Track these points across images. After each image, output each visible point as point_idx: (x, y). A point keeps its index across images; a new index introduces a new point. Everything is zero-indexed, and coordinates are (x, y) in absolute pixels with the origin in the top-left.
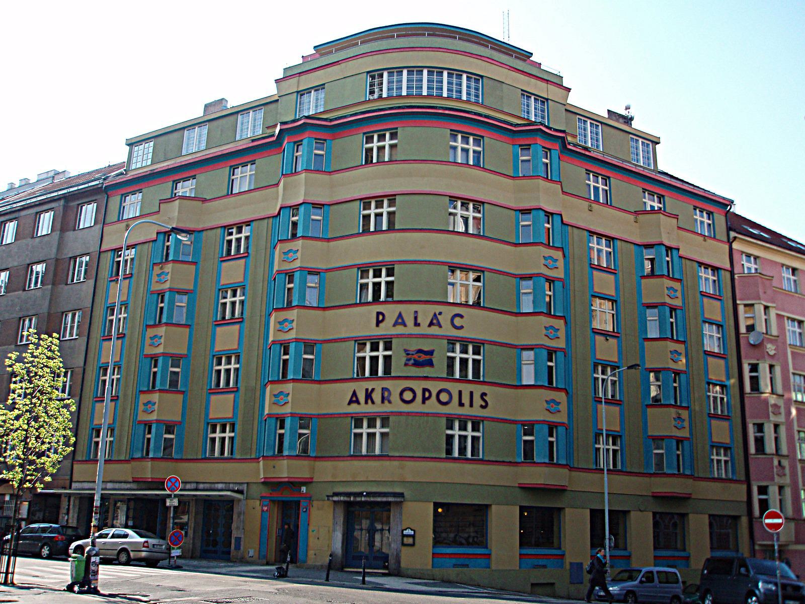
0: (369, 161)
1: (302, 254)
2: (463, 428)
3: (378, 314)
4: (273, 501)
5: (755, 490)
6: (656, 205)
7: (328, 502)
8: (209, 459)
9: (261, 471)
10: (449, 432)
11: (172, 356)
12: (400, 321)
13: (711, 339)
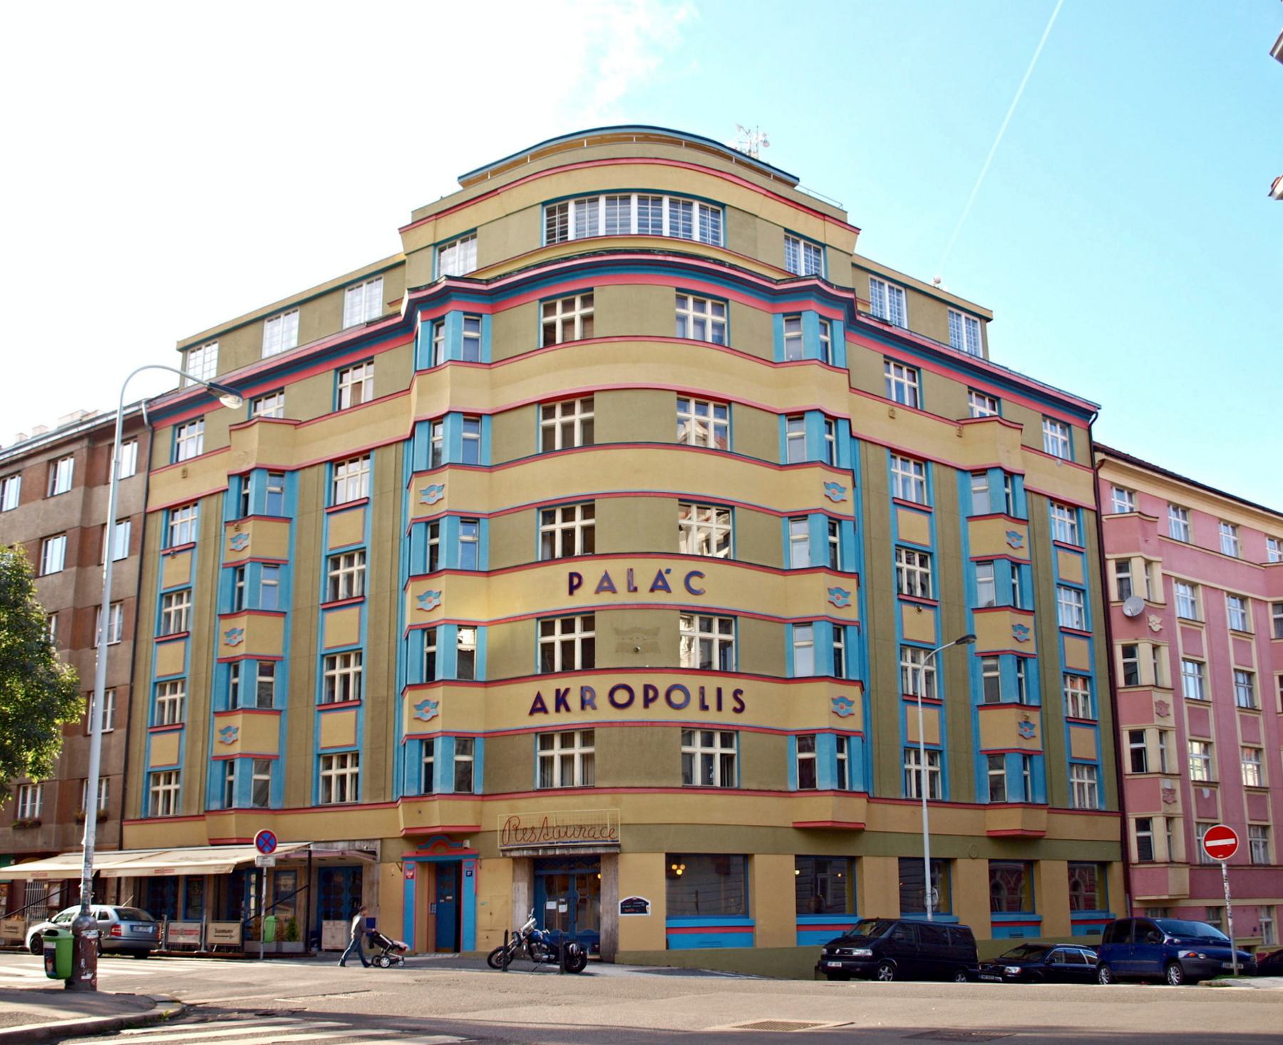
0: (549, 340)
1: (453, 492)
2: (708, 742)
3: (572, 575)
4: (422, 864)
5: (1132, 825)
6: (988, 411)
7: (505, 860)
9: (400, 820)
10: (686, 749)
11: (259, 658)
12: (606, 584)
13: (1069, 612)
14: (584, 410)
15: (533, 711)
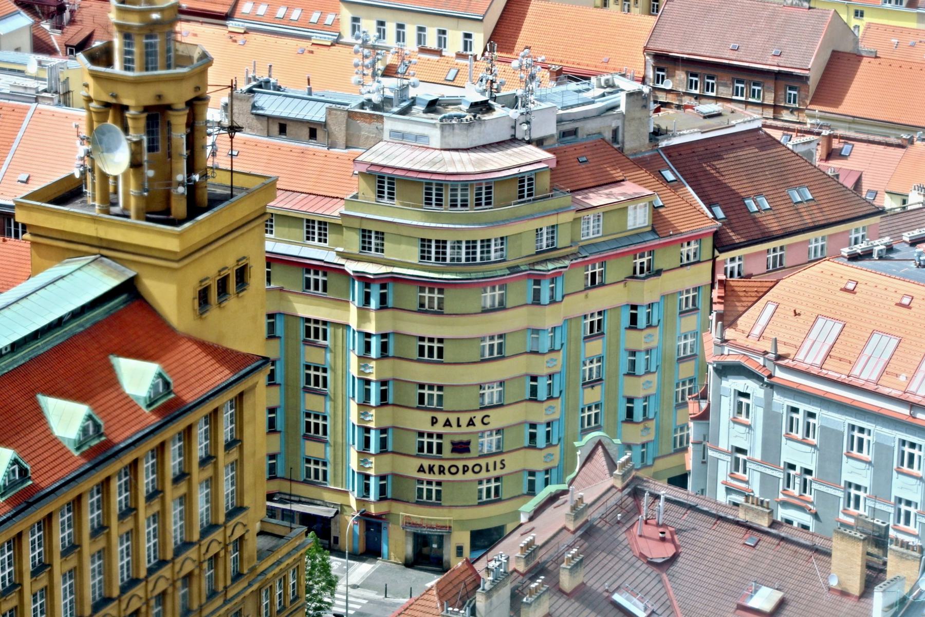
3: (433, 418)
14: (439, 293)
15: (419, 471)
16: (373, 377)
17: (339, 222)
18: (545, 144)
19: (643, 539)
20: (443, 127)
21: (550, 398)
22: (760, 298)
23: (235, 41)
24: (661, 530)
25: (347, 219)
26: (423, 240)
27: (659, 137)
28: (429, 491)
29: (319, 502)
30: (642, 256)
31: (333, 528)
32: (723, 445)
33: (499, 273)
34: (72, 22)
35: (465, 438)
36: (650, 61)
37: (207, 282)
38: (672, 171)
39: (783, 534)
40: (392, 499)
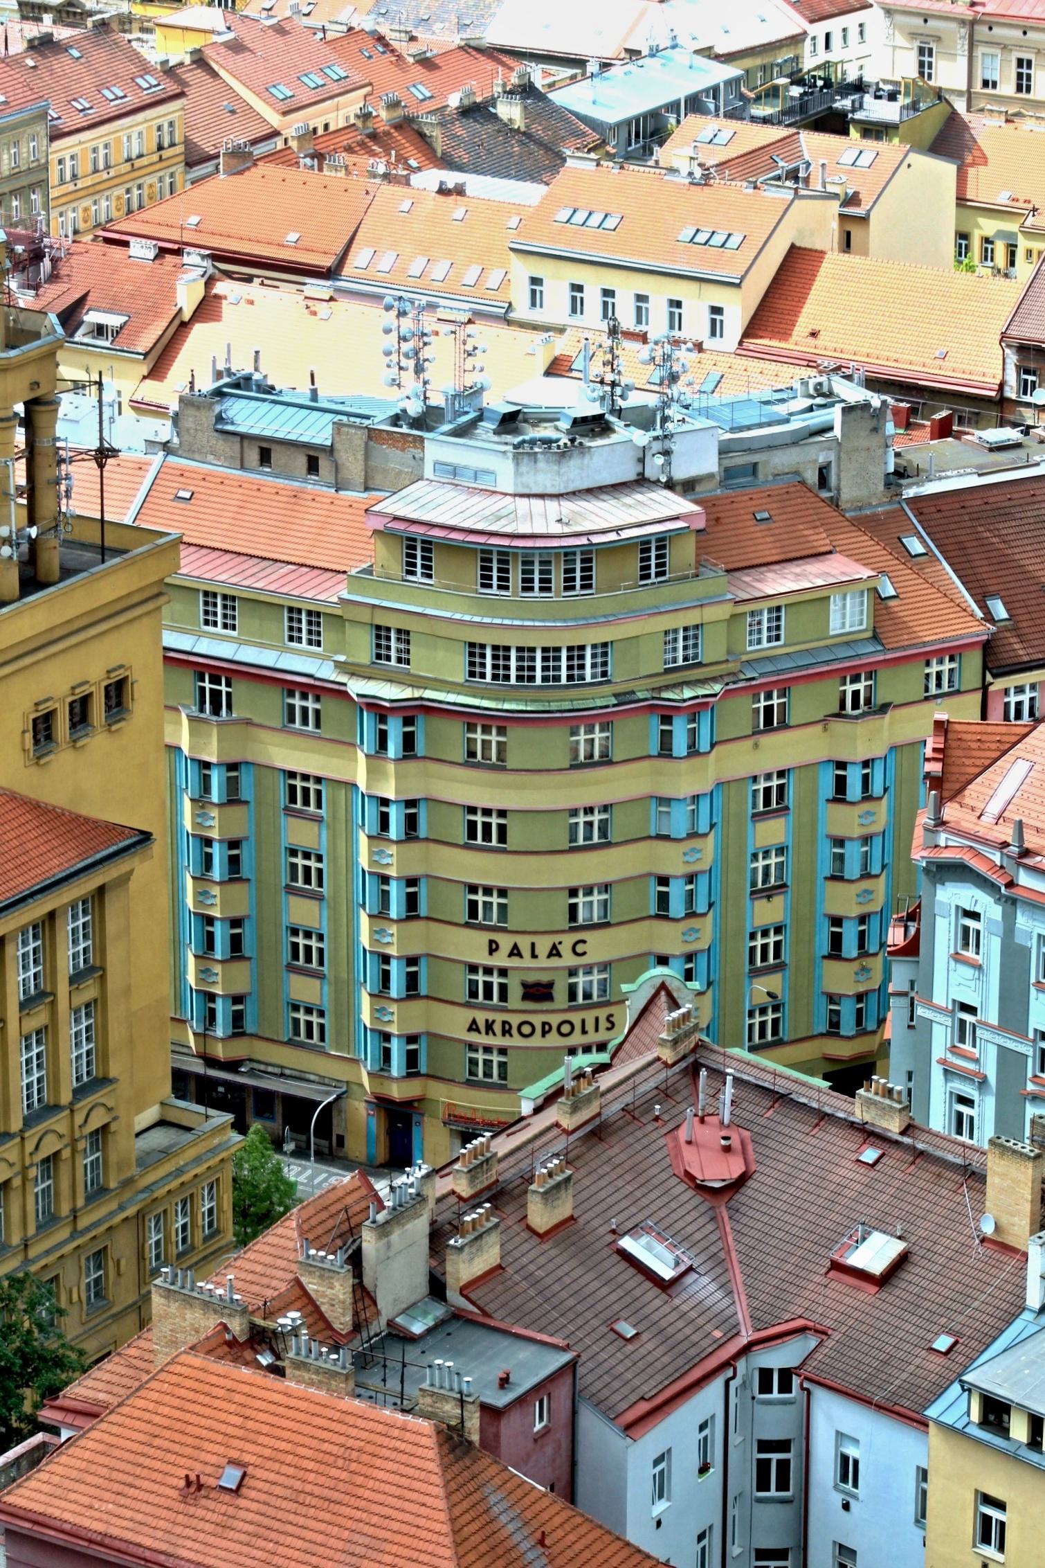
8: (936, 697)
15: (470, 1029)
16: (392, 872)
17: (339, 612)
18: (698, 489)
19: (692, 1149)
20: (517, 458)
21: (691, 915)
22: (1005, 753)
23: (314, 313)
24: (724, 1133)
25: (351, 607)
26: (472, 645)
27: (903, 482)
28: (488, 1063)
29: (312, 1077)
30: (856, 679)
31: (335, 1122)
32: (939, 998)
33: (599, 703)
34: (54, 277)
35: (544, 978)
36: (1012, 358)
37: (50, 706)
38: (920, 537)
39: (920, 1146)
40: (428, 1076)
